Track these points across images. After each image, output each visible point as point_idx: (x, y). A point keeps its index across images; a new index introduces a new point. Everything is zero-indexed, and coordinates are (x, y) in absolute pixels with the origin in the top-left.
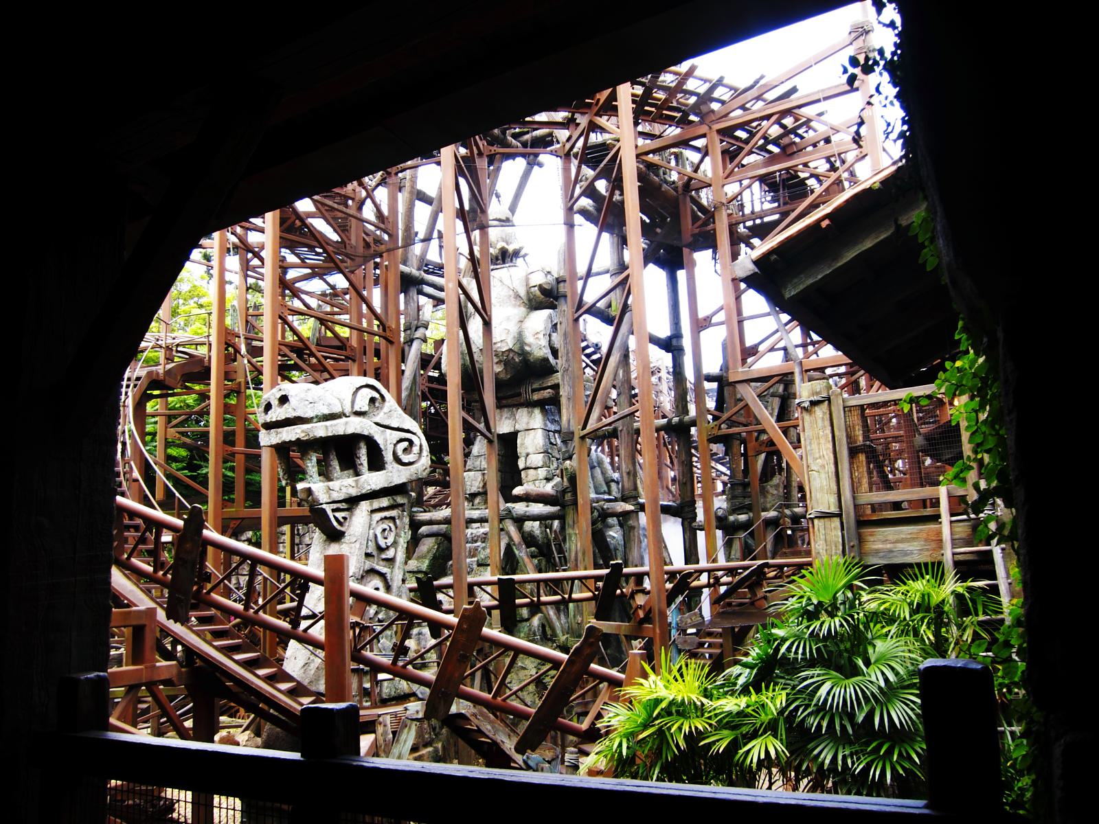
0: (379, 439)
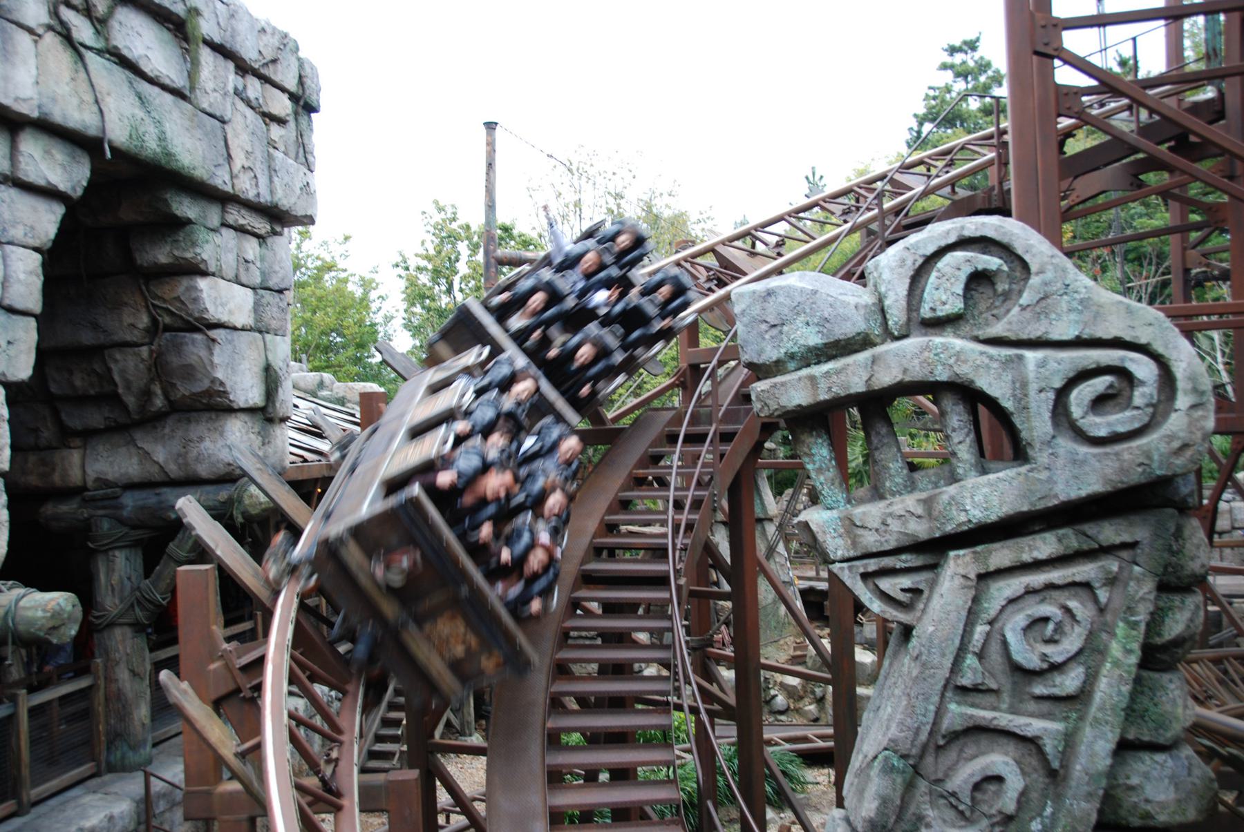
0: (995, 385)
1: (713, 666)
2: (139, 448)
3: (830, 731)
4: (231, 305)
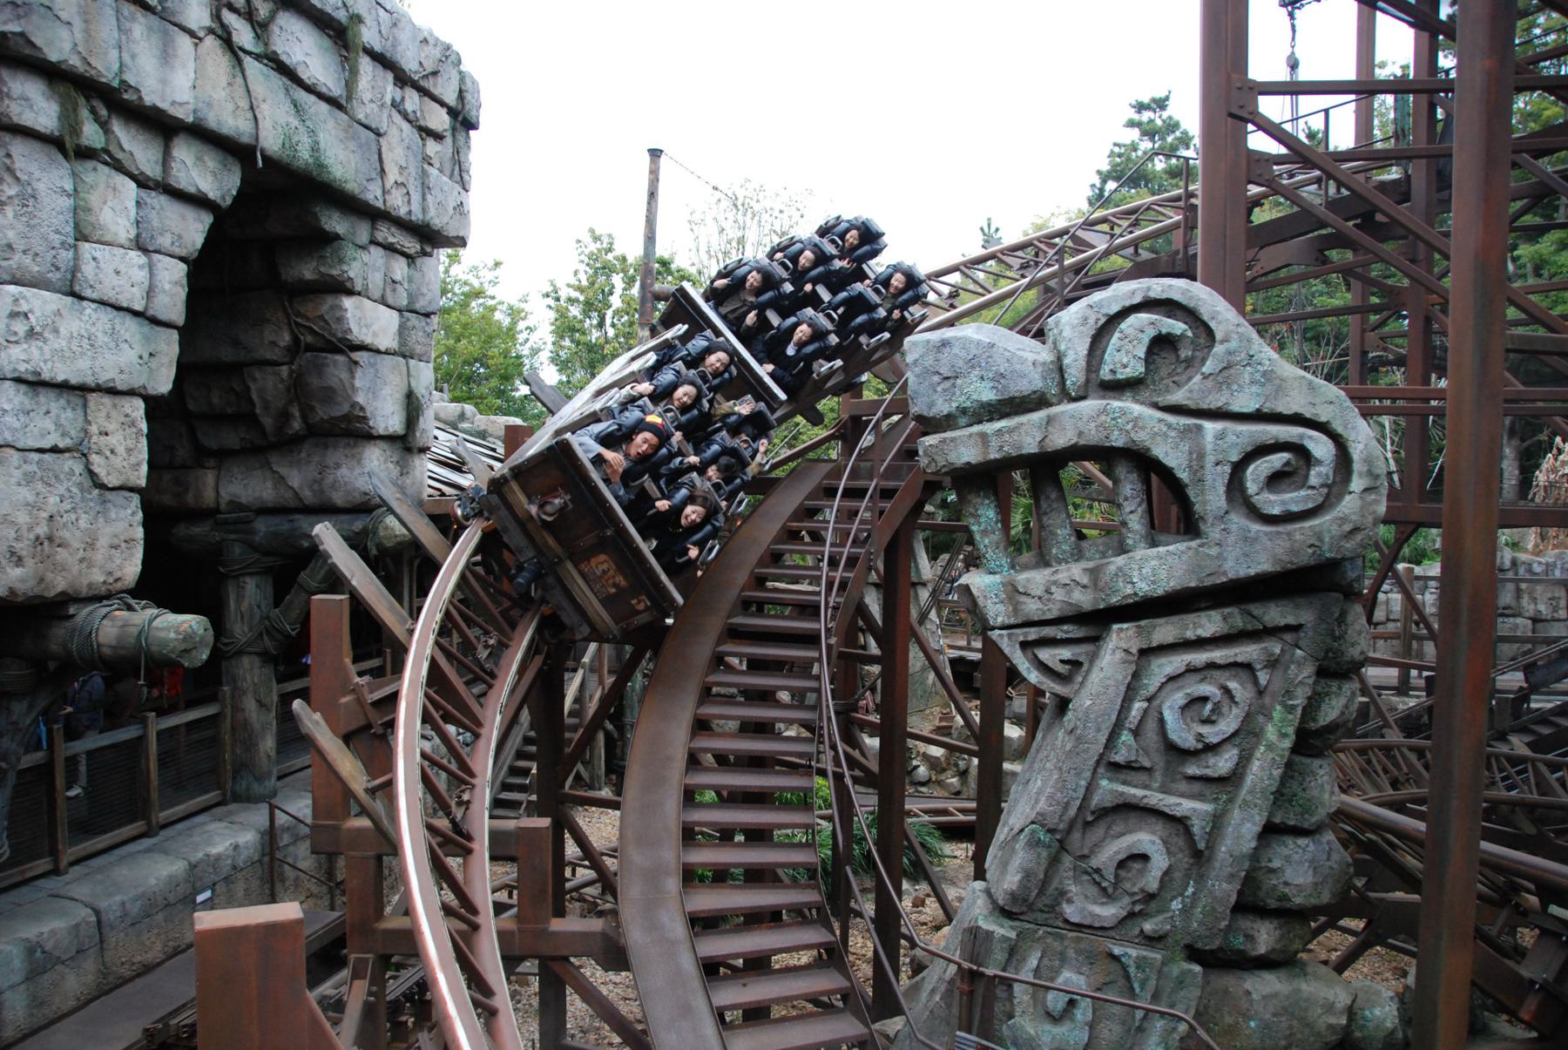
0: (1171, 455)
1: (857, 732)
2: (274, 472)
3: (973, 805)
4: (375, 327)
